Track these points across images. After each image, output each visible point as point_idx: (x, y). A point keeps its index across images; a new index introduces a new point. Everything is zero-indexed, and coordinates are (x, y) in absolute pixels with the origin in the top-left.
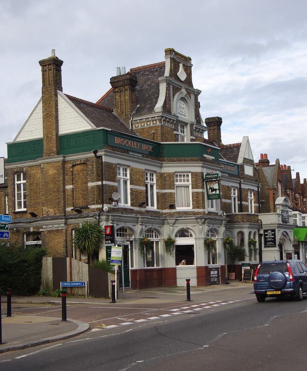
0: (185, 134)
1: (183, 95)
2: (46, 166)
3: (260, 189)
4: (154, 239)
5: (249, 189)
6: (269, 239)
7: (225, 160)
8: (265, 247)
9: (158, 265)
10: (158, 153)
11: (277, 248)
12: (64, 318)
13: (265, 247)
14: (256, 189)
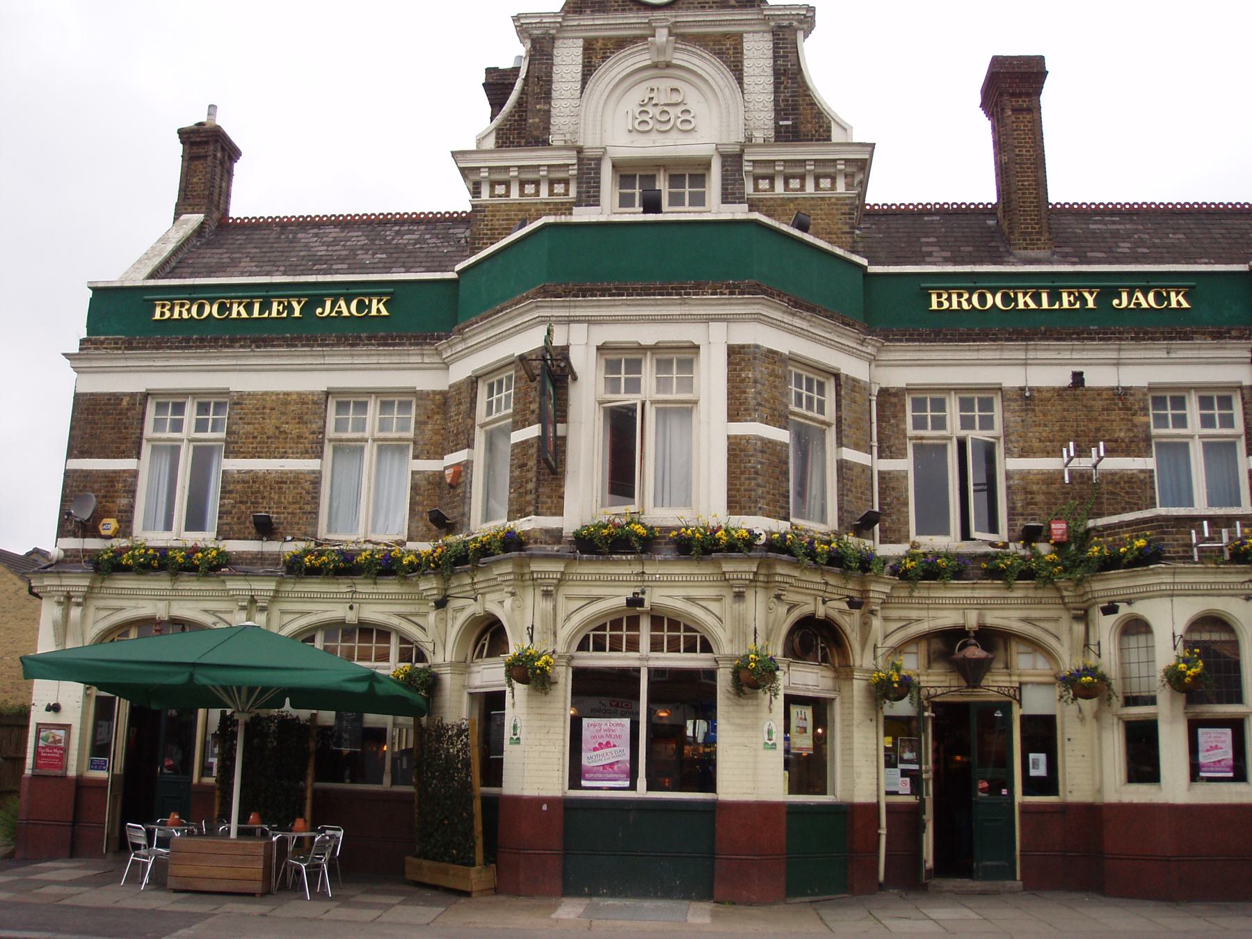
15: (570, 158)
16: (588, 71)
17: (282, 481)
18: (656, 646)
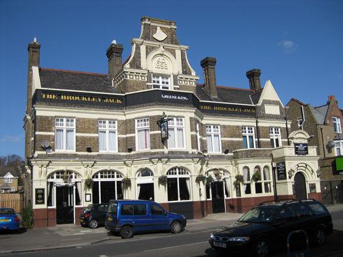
6: (281, 172)
13: (279, 179)
15: (146, 72)
16: (147, 53)
17: (90, 139)
18: (179, 173)
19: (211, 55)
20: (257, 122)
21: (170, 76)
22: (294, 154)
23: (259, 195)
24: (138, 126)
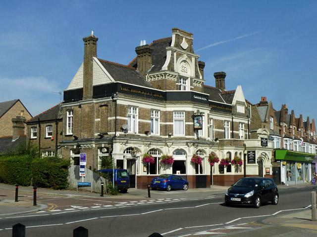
0: (187, 85)
1: (184, 59)
2: (75, 107)
3: (249, 122)
4: (202, 156)
5: (240, 123)
6: (251, 158)
7: (225, 104)
8: (248, 163)
9: (201, 173)
10: (163, 97)
11: (257, 164)
12: (35, 204)
13: (248, 163)
14: (247, 122)
19: (219, 70)
20: (232, 118)
21: (188, 78)
22: (260, 146)
23: (229, 174)
24: (176, 117)
